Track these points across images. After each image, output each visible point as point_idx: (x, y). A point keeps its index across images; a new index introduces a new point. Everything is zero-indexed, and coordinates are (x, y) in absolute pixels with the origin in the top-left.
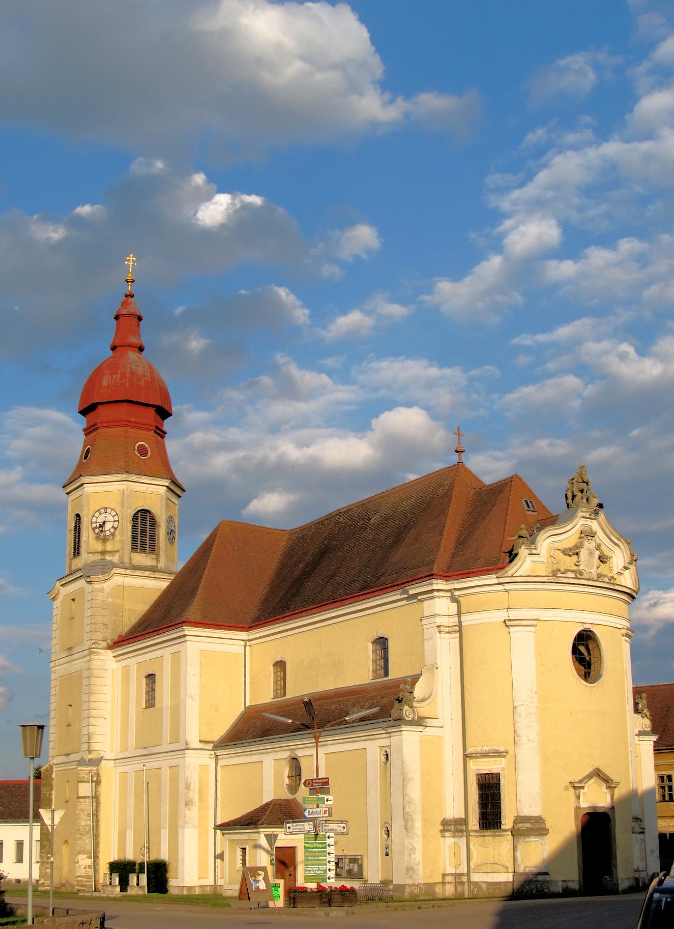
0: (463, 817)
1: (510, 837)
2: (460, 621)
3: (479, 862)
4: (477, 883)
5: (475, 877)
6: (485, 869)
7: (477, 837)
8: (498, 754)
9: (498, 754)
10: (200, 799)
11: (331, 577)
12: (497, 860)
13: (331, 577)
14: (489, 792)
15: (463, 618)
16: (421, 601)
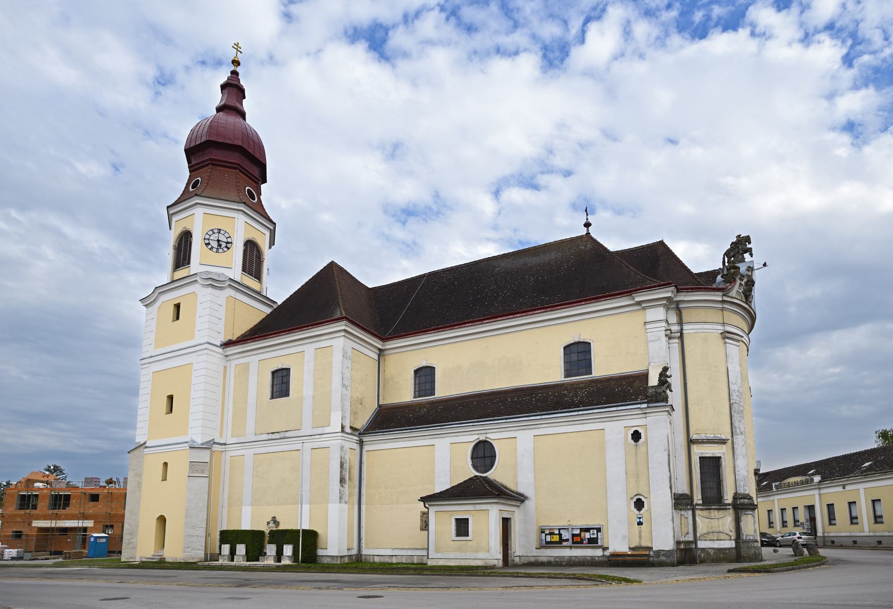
0: (687, 491)
1: (731, 511)
2: (682, 329)
3: (705, 531)
4: (703, 549)
5: (701, 544)
6: (710, 537)
7: (702, 510)
8: (723, 442)
9: (723, 442)
10: (349, 479)
11: (638, 476)
12: (721, 529)
13: (638, 476)
14: (711, 468)
15: (685, 327)
16: (644, 309)
